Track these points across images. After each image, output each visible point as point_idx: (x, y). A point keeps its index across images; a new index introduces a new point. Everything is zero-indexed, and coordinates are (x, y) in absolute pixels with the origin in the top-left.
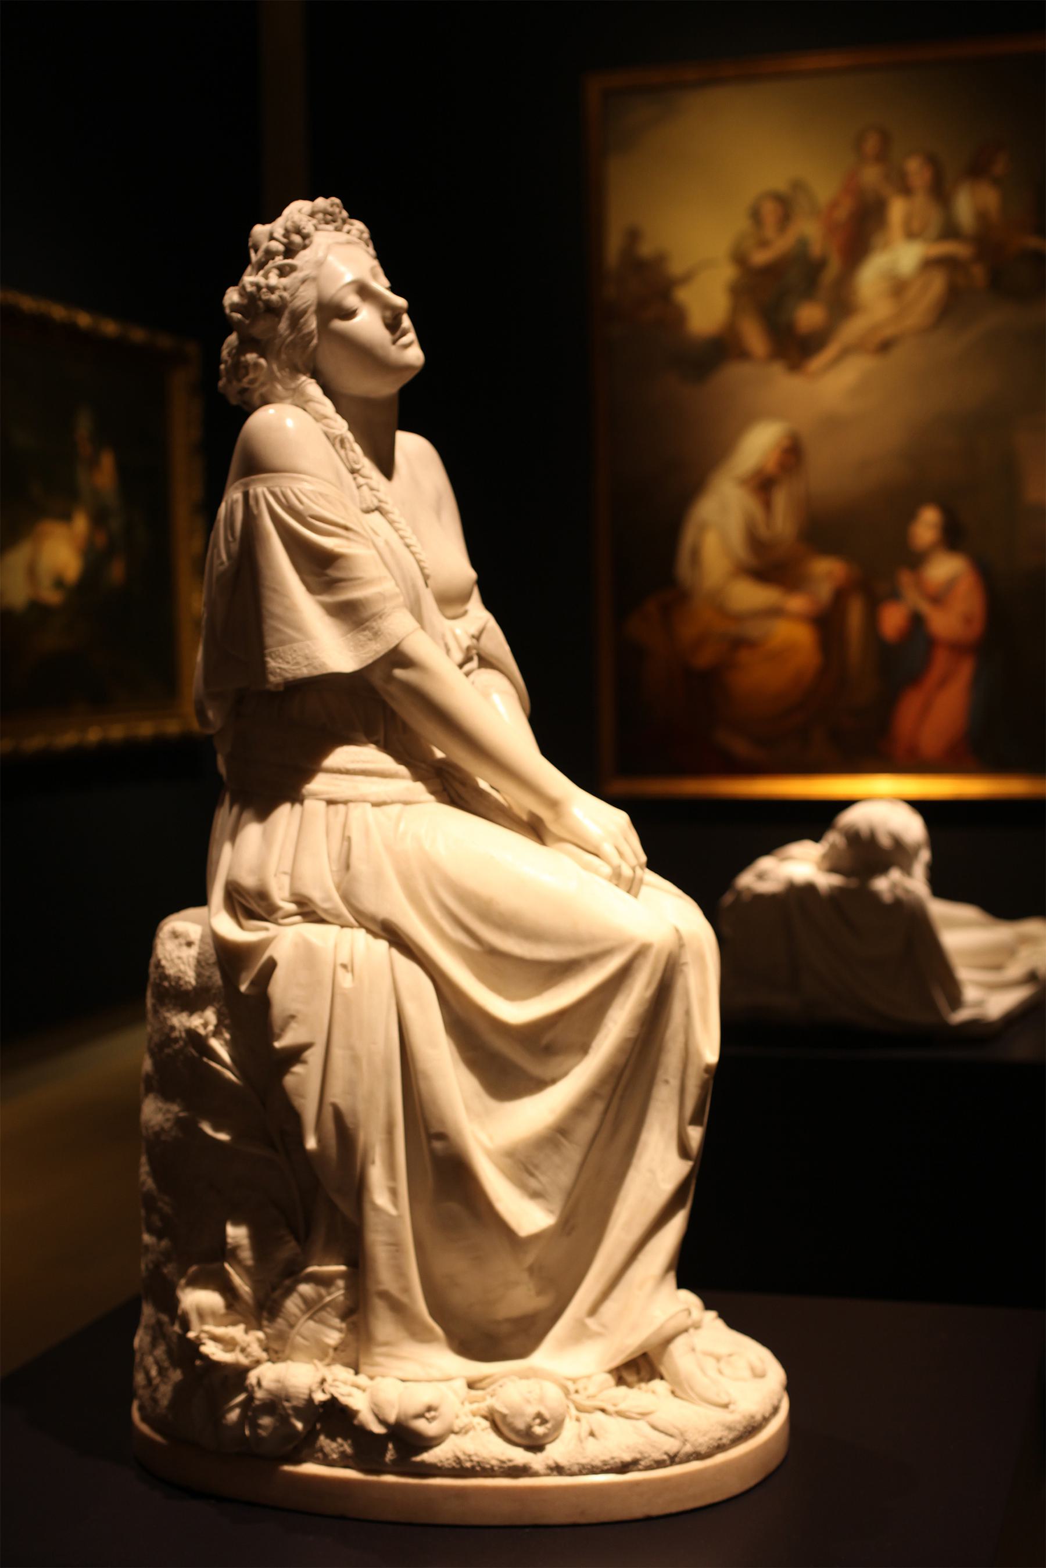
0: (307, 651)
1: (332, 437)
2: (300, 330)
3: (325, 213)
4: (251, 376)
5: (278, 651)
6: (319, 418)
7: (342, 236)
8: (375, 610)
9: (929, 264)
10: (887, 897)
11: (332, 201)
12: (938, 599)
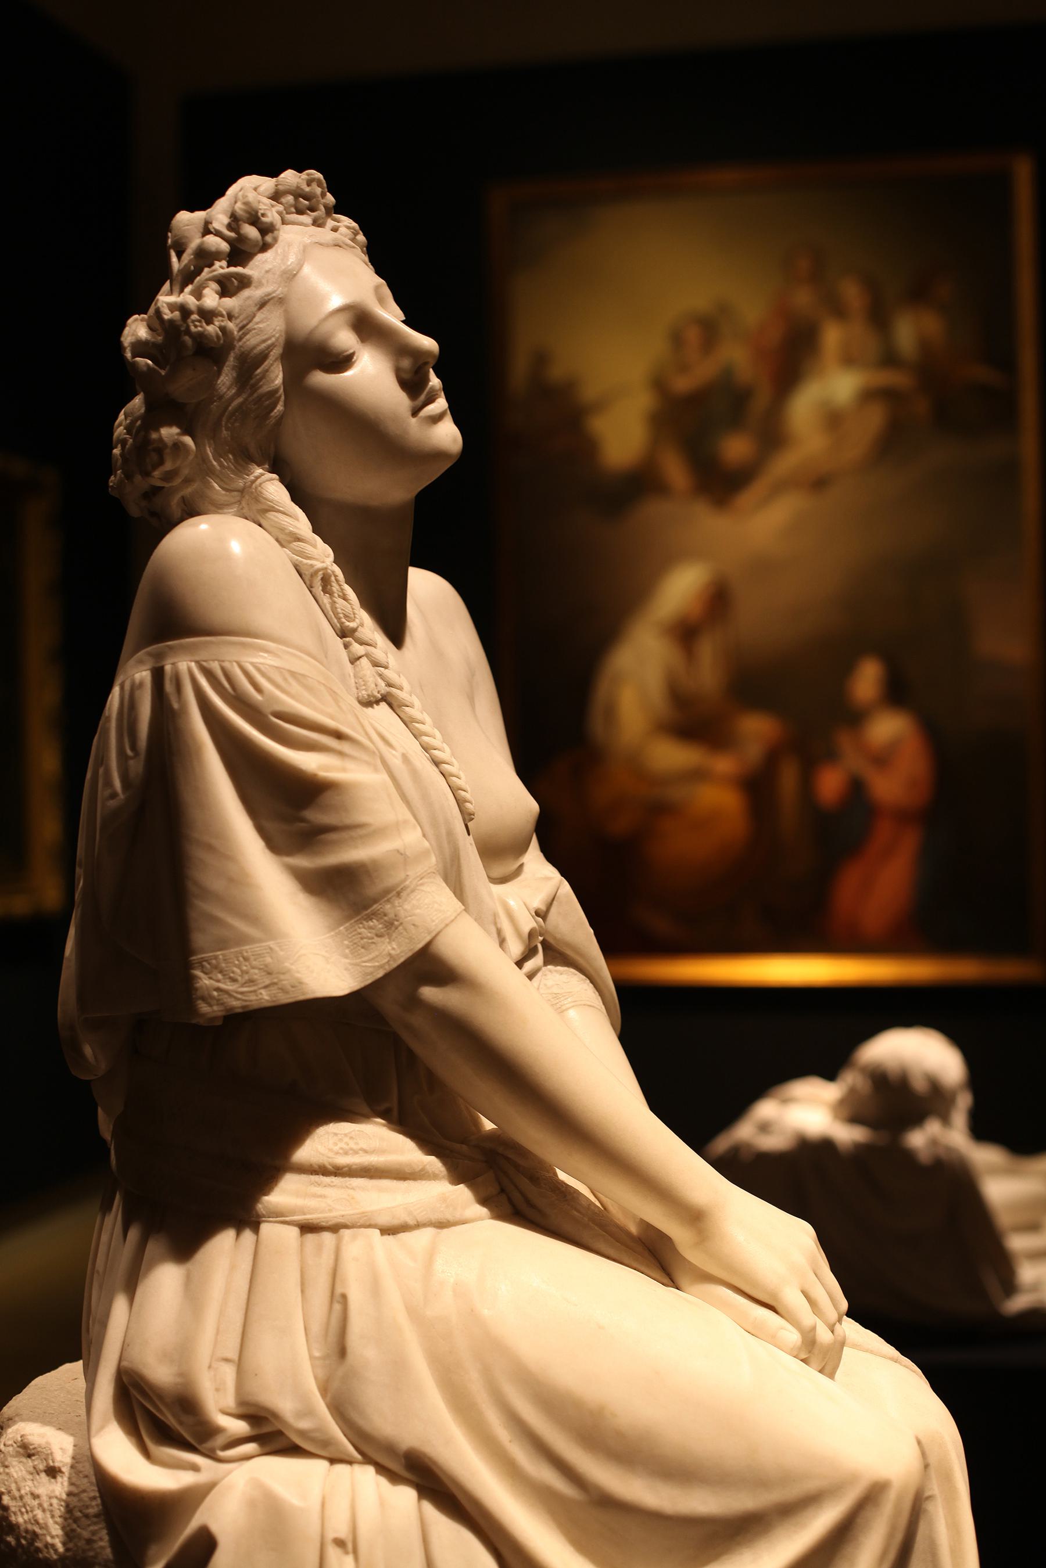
0: (268, 960)
1: (307, 573)
2: (255, 388)
3: (298, 194)
4: (168, 466)
5: (216, 958)
6: (286, 539)
7: (325, 234)
8: (390, 882)
9: (868, 396)
10: (925, 1156)
11: (308, 175)
12: (882, 759)
